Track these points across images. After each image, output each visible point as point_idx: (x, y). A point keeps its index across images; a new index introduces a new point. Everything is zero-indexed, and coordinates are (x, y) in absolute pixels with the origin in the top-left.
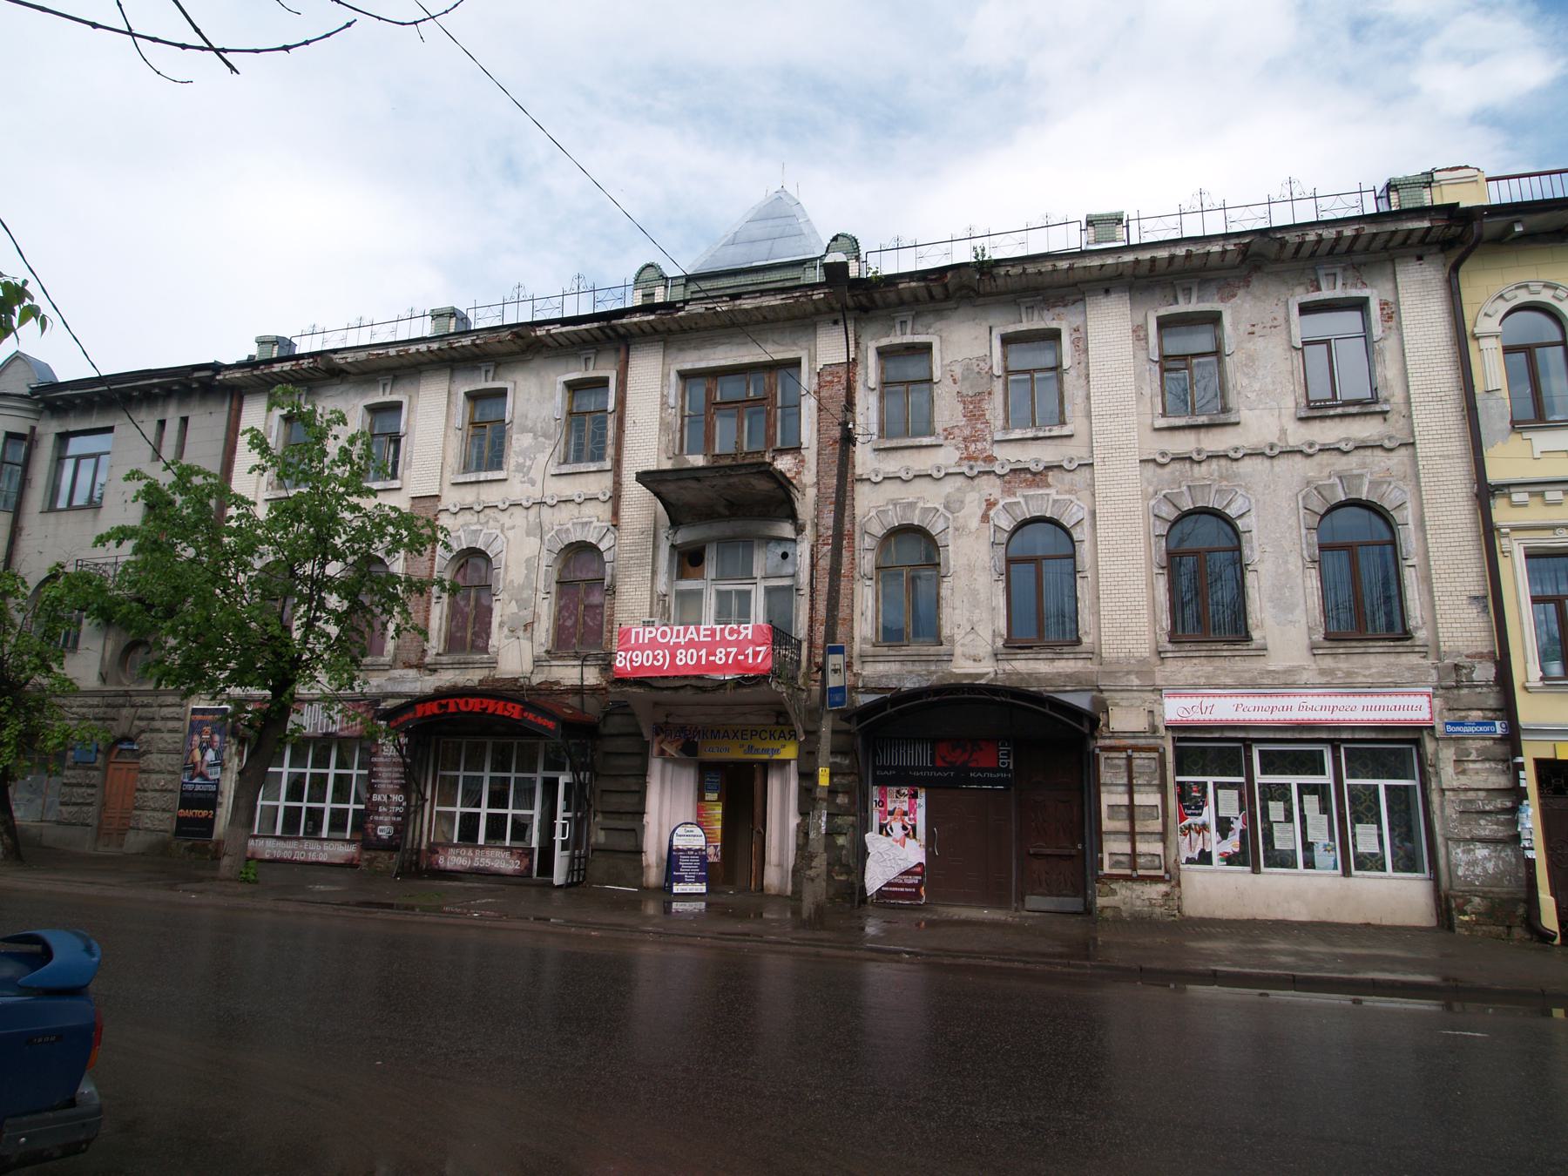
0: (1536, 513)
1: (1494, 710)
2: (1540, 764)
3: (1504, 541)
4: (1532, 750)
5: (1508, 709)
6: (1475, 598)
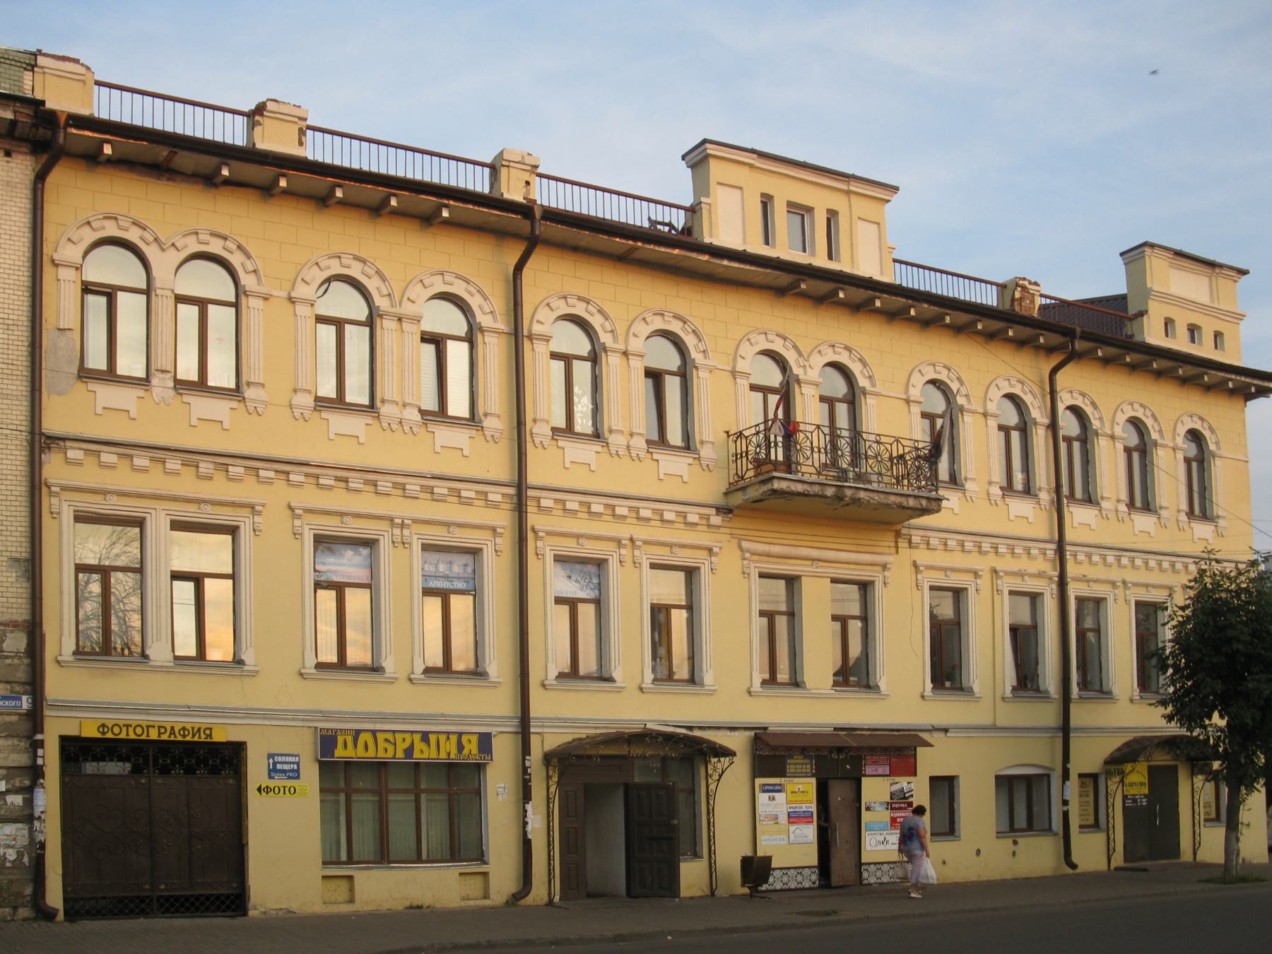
0: (89, 475)
1: (24, 683)
2: (64, 740)
3: (54, 501)
4: (55, 729)
5: (35, 684)
6: (17, 560)
